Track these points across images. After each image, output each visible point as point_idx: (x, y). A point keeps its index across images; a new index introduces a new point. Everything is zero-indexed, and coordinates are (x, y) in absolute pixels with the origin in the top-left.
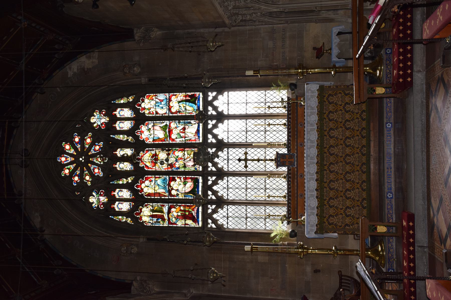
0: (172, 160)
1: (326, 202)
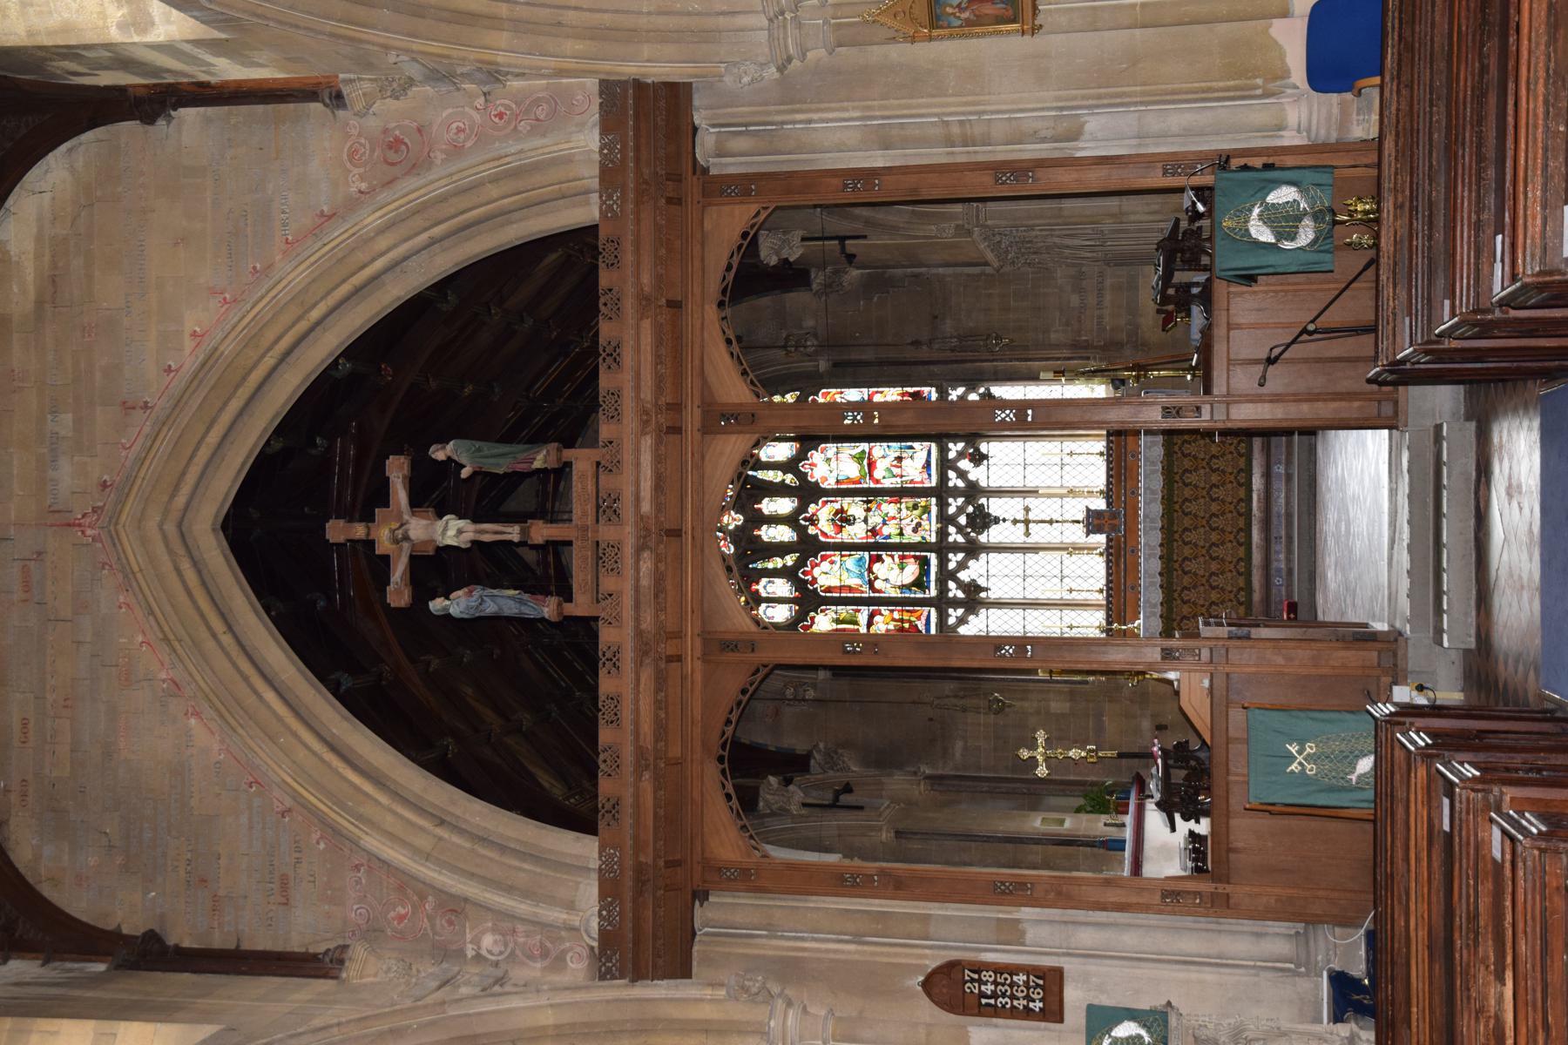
0: (875, 519)
1: (1176, 595)
